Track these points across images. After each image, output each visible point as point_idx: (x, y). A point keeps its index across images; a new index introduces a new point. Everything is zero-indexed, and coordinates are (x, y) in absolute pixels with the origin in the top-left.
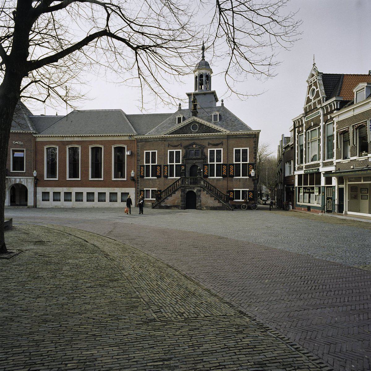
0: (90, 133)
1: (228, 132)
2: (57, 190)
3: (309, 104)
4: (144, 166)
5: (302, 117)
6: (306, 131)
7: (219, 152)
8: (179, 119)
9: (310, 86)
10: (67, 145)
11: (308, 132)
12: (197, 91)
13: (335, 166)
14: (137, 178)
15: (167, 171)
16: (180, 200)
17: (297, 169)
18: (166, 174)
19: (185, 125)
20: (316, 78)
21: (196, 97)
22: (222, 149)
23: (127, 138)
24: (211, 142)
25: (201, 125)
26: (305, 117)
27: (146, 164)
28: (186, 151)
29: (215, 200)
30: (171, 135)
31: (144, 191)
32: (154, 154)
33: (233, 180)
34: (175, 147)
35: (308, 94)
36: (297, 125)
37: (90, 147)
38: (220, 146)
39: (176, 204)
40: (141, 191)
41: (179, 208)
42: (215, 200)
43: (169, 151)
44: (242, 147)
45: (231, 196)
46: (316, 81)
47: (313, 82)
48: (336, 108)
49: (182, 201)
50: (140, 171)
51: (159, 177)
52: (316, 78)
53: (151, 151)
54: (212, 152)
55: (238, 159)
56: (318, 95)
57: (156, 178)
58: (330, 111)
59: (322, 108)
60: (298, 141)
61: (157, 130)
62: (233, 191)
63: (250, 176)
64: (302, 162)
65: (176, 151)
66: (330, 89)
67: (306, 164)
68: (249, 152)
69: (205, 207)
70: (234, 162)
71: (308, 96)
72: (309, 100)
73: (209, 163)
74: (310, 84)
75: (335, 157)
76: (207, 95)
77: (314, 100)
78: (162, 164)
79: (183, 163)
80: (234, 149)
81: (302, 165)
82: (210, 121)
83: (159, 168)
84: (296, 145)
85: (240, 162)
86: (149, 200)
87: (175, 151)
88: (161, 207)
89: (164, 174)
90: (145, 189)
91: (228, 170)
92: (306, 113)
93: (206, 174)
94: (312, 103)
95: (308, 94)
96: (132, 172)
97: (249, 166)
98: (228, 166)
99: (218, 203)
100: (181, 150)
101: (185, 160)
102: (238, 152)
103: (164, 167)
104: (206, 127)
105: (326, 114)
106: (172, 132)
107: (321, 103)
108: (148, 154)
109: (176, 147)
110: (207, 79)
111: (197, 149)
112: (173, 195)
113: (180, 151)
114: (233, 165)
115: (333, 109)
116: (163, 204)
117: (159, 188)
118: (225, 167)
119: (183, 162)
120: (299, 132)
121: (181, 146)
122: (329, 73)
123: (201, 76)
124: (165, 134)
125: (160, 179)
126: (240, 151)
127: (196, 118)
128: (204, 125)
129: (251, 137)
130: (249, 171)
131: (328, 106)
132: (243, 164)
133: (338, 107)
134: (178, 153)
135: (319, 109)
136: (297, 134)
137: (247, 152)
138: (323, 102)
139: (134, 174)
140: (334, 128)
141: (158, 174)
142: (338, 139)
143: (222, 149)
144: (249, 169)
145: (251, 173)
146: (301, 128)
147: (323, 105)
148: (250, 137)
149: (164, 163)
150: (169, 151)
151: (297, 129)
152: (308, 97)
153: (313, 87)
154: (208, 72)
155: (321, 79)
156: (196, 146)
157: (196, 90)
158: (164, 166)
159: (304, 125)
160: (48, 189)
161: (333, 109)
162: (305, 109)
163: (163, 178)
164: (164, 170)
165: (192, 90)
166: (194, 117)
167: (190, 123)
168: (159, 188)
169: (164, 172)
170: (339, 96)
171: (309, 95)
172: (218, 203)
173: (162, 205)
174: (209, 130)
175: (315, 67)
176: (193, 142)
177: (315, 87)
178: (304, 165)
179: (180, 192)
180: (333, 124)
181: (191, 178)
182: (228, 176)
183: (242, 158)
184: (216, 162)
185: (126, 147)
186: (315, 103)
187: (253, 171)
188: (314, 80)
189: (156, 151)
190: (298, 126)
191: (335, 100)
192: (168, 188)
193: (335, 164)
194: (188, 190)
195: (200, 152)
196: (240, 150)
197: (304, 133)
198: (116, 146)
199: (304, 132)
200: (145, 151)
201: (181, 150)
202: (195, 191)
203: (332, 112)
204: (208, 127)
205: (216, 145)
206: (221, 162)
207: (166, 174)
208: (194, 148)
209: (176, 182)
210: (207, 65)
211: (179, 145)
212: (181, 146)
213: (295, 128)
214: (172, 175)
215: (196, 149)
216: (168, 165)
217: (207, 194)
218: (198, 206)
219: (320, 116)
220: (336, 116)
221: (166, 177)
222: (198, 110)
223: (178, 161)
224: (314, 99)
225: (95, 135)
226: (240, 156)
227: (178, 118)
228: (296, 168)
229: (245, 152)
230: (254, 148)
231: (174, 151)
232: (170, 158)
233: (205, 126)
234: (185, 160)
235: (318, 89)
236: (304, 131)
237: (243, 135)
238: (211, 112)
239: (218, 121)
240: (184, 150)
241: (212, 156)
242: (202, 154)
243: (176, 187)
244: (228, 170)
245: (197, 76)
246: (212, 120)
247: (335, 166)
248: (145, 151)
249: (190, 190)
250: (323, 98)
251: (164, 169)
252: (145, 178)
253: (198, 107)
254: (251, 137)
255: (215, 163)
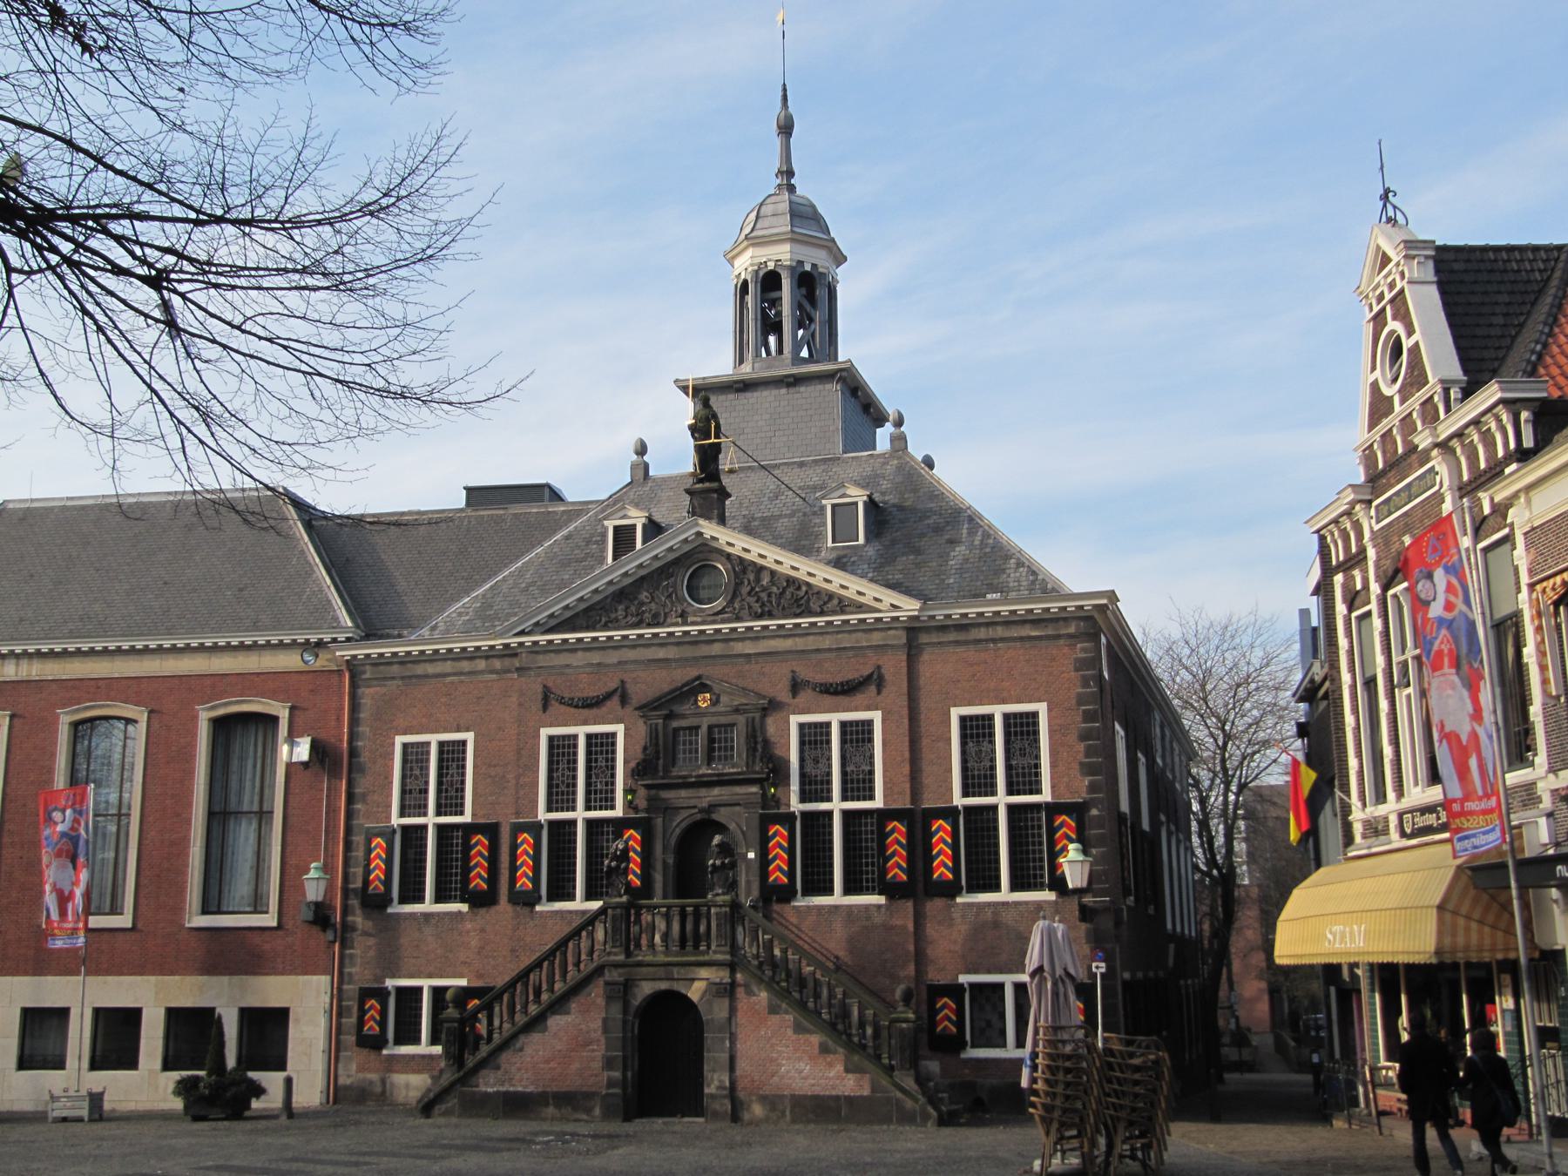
0: (73, 635)
1: (910, 606)
2: (117, 992)
3: (1385, 425)
4: (789, 819)
5: (1353, 504)
6: (1385, 588)
7: (857, 735)
8: (624, 537)
9: (1379, 320)
10: (64, 706)
11: (1395, 596)
12: (747, 368)
13: (1550, 815)
14: (346, 910)
15: (527, 870)
16: (599, 1054)
17: (1364, 837)
18: (524, 883)
19: (643, 572)
20: (1402, 275)
21: (715, 402)
22: (876, 717)
23: (290, 661)
24: (805, 673)
25: (743, 568)
26: (1370, 502)
27: (824, 806)
28: (653, 734)
29: (824, 1049)
30: (557, 637)
31: (381, 994)
32: (451, 755)
33: (956, 915)
34: (590, 705)
35: (1373, 369)
36: (1338, 555)
37: (204, 717)
38: (859, 698)
39: (572, 1083)
40: (937, 991)
41: (589, 1111)
42: (824, 1049)
43: (545, 733)
44: (1004, 702)
45: (946, 1026)
46: (1402, 291)
47: (1388, 297)
48: (1512, 445)
49: (609, 1063)
50: (368, 861)
51: (482, 900)
52: (1402, 275)
53: (998, 711)
54: (814, 737)
55: (978, 781)
56: (1417, 377)
57: (464, 907)
58: (1489, 469)
59: (1444, 446)
60: (1351, 652)
61: (486, 603)
62: (956, 991)
63: (1058, 884)
64: (1381, 797)
65: (1006, 717)
66: (1493, 332)
67: (1406, 803)
68: (1052, 732)
69: (763, 1099)
70: (959, 800)
71: (1371, 379)
72: (1379, 407)
73: (796, 805)
74: (1376, 309)
75: (1541, 759)
76: (804, 390)
77: (1402, 402)
78: (506, 822)
79: (636, 809)
80: (956, 713)
81: (1381, 810)
82: (803, 543)
83: (480, 842)
84: (1346, 678)
85: (574, 809)
86: (413, 1057)
87: (581, 731)
88: (479, 1106)
89: (513, 880)
90: (390, 983)
91: (919, 850)
92: (1376, 480)
93: (777, 876)
94: (1391, 422)
95: (1373, 369)
96: (313, 874)
97: (1050, 821)
98: (918, 821)
99: (847, 1070)
100: (619, 729)
101: (648, 787)
102: (976, 729)
103: (514, 837)
104: (772, 582)
105: (1470, 482)
106: (568, 614)
107: (1436, 418)
108: (414, 755)
109: (594, 711)
110: (811, 298)
111: (723, 720)
112: (555, 1022)
113: (614, 735)
114: (950, 813)
115: (1501, 453)
116: (488, 1084)
117: (480, 976)
118: (897, 832)
119: (629, 805)
120: (1353, 599)
121: (624, 700)
122: (1461, 243)
123: (770, 281)
124: (522, 633)
125: (487, 915)
126: (992, 726)
127: (709, 529)
128: (763, 568)
129: (1058, 637)
130: (1053, 856)
131: (1476, 438)
132: (846, 814)
133: (1528, 442)
134: (601, 746)
135: (1425, 457)
136: (1341, 608)
137: (1036, 733)
138: (1448, 409)
139: (323, 884)
140: (1516, 569)
141: (479, 882)
142: (1389, 644)
143: (876, 717)
144: (1052, 843)
145: (1067, 869)
146: (1357, 573)
147: (1446, 429)
148: (1048, 637)
149: (517, 814)
150: (545, 733)
151: (1339, 579)
152: (1375, 386)
153: (1393, 325)
154: (813, 258)
155: (1430, 275)
156: (715, 702)
157: (741, 360)
158: (518, 829)
159: (1371, 553)
160: (52, 991)
161: (1501, 453)
162: (1368, 457)
163: (509, 908)
164: (466, 858)
165: (720, 363)
166: (701, 521)
167: (676, 562)
168: (480, 976)
169: (513, 868)
170: (1532, 372)
171: (1378, 372)
172: (847, 1070)
173: (483, 1089)
174: (844, 605)
175: (1391, 213)
176: (682, 675)
177: (1398, 327)
178: (1390, 807)
179: (601, 1001)
180: (1507, 546)
181: (669, 907)
182: (921, 886)
183: (1009, 767)
184: (845, 798)
185: (284, 714)
186: (1407, 421)
187: (1073, 852)
188: (1392, 286)
189: (469, 736)
190: (1346, 561)
191: (1502, 401)
192: (524, 976)
193: (1547, 803)
194: (646, 989)
195: (738, 739)
196: (828, 725)
197: (1373, 606)
198: (221, 712)
199: (1373, 598)
200: (400, 740)
201: (619, 729)
202: (695, 992)
203: (1494, 473)
204: (791, 581)
205: (844, 691)
206: (613, 808)
207: (524, 883)
208: (703, 714)
209: (576, 933)
210: (805, 217)
211: (608, 696)
212: (624, 700)
213: (1328, 571)
214: (561, 890)
215: (714, 720)
216: (792, 816)
217: (773, 1010)
218: (712, 1096)
219: (1439, 498)
220: (1516, 495)
221: (527, 900)
222: (726, 481)
223: (599, 795)
224: (1405, 395)
225: (194, 643)
226: (993, 760)
227: (616, 529)
228: (1358, 829)
229: (1022, 727)
230: (1079, 703)
231: (990, 717)
232: (550, 778)
233: (773, 573)
234: (648, 787)
235: (1416, 337)
236: (1375, 588)
237: (1023, 622)
238: (823, 488)
239: (861, 540)
240: (641, 729)
241: (816, 761)
242: (752, 750)
243: (577, 964)
244: (919, 850)
245: (745, 283)
246: (820, 536)
247: (1550, 815)
248: (400, 740)
249: (664, 986)
250: (1446, 391)
251: (514, 847)
252: (396, 908)
253: (726, 462)
254: (1058, 637)
255: (1002, 799)
